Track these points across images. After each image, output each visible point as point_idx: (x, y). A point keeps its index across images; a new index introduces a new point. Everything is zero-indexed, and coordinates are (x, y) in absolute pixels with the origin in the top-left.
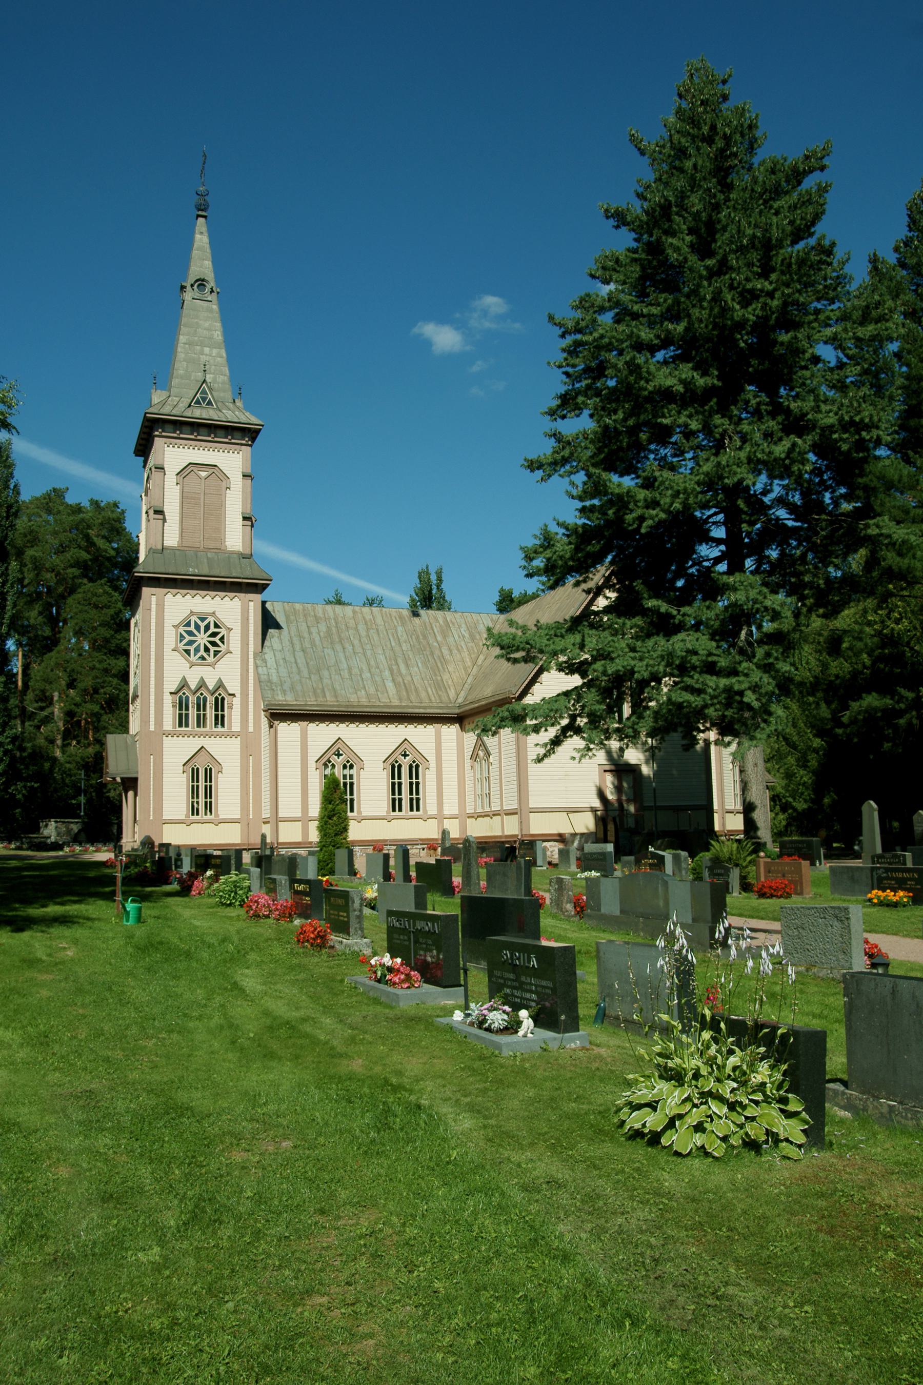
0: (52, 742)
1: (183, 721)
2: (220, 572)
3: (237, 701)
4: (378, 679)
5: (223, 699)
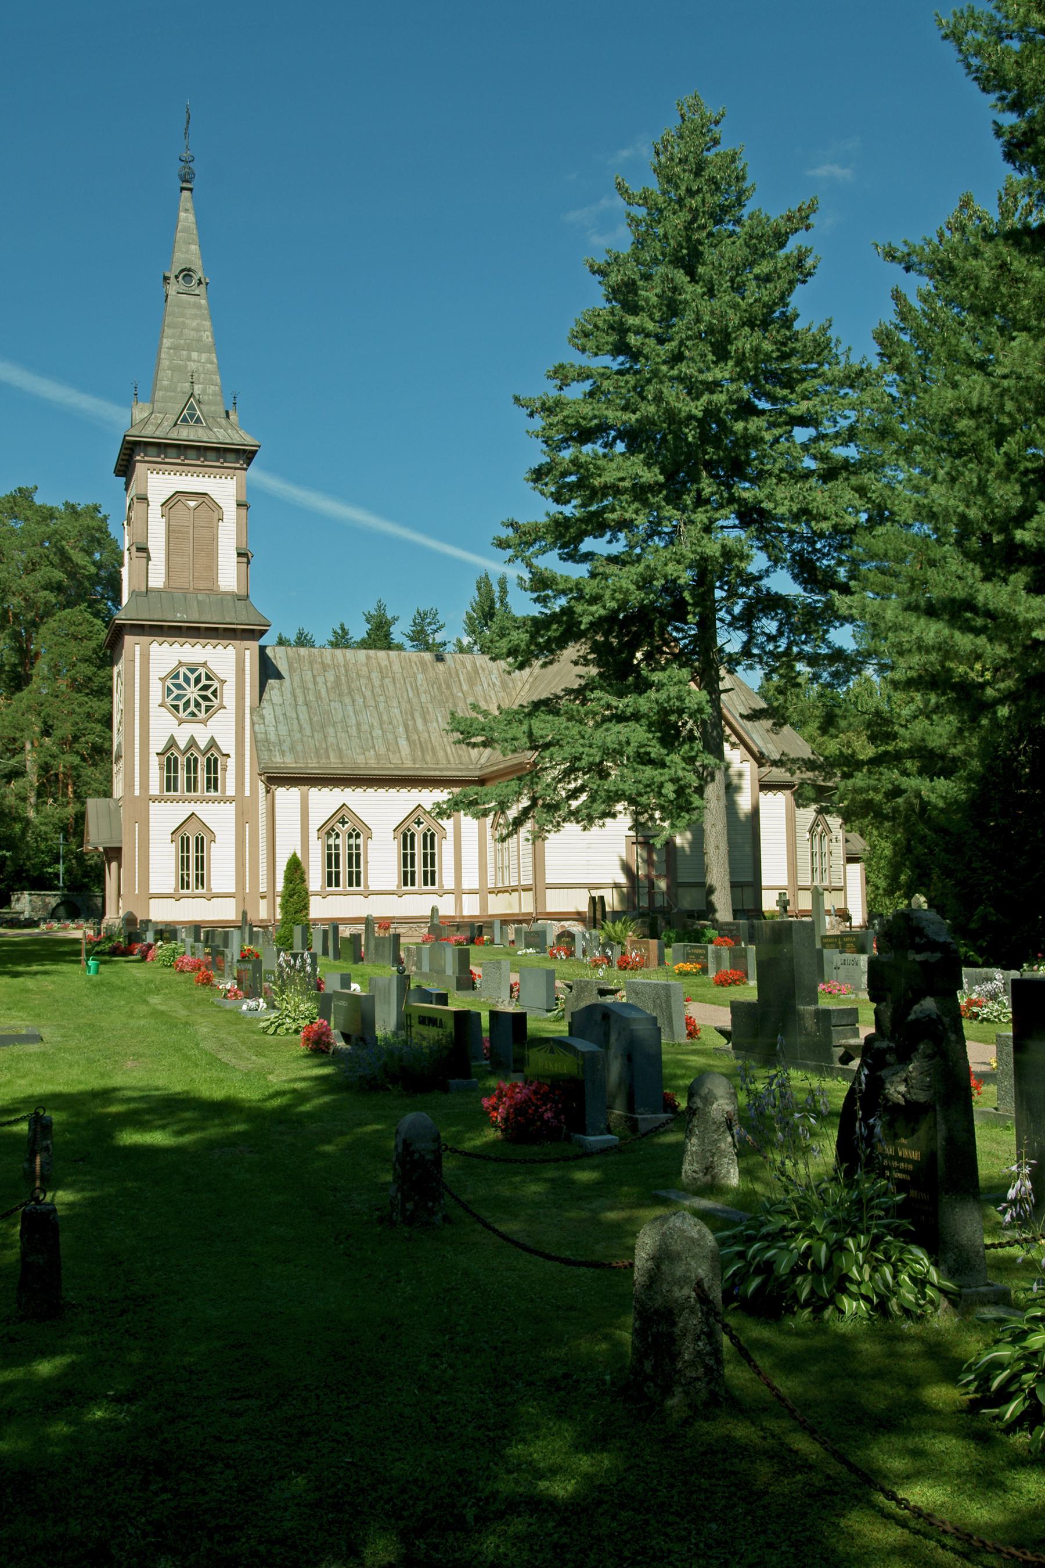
0: (24, 799)
1: (171, 784)
2: (212, 617)
3: (231, 763)
4: (390, 736)
5: (216, 760)
